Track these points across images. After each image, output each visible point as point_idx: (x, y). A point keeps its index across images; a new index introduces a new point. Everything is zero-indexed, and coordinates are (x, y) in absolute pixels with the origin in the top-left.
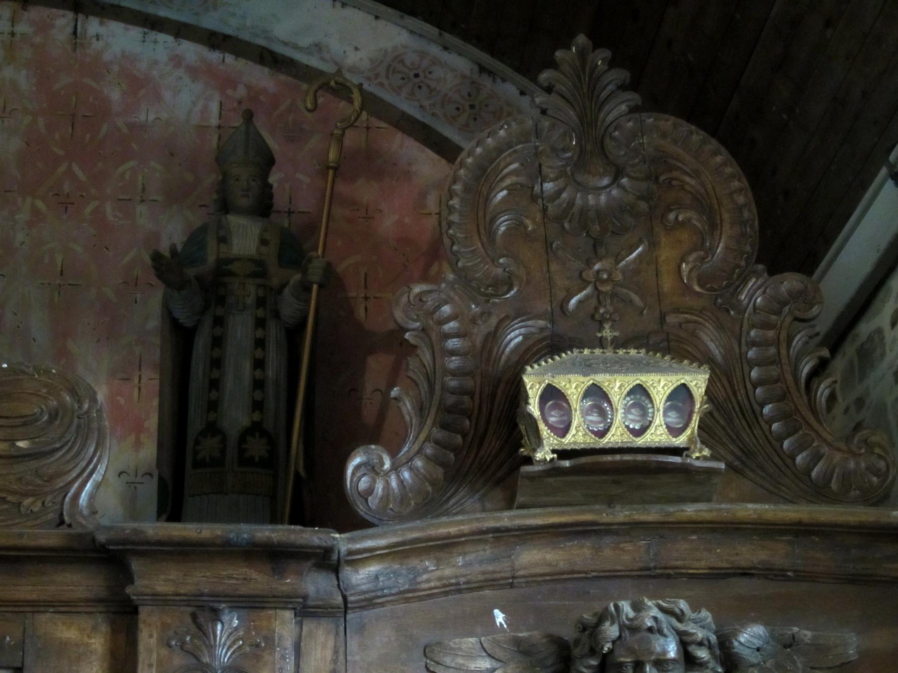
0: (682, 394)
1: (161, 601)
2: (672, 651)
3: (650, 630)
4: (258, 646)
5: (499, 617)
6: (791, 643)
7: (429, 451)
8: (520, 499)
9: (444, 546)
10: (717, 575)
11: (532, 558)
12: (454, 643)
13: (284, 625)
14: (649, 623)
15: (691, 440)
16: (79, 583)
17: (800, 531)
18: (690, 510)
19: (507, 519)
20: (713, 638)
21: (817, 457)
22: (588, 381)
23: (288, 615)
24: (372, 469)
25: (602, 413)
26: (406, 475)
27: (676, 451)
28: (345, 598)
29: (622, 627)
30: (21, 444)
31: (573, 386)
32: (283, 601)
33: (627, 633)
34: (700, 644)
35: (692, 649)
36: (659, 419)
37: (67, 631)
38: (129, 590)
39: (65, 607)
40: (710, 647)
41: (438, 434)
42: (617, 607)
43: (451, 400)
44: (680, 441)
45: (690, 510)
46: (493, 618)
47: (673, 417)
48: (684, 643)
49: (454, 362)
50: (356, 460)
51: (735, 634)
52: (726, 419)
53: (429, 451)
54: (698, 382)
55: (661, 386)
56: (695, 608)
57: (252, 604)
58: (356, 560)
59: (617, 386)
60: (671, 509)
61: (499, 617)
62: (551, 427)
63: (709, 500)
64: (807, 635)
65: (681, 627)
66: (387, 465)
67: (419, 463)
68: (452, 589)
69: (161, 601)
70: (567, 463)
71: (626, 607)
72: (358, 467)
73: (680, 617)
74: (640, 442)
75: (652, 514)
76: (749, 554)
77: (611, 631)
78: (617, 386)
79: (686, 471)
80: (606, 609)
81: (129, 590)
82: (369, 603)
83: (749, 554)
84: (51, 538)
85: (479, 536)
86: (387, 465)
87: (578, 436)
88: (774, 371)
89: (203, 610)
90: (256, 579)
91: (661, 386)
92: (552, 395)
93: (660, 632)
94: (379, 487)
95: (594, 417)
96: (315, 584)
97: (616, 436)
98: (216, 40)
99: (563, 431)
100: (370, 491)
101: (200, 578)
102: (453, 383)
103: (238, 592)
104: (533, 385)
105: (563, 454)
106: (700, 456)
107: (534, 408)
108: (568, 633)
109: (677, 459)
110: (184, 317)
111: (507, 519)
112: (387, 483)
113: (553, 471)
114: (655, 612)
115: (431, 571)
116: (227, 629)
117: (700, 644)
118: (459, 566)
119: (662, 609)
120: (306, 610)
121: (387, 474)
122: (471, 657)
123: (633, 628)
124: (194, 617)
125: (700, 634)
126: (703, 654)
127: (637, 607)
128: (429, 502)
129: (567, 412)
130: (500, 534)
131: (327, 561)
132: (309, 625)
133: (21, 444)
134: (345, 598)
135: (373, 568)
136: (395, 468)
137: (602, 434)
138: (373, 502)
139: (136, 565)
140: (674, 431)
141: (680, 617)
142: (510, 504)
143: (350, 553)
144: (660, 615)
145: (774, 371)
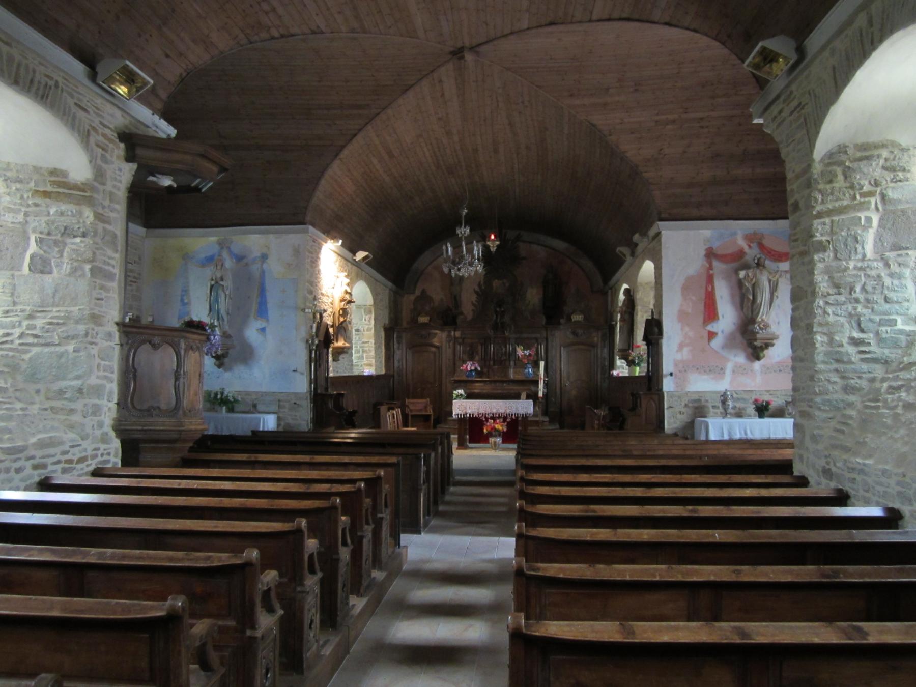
98: (546, 246)
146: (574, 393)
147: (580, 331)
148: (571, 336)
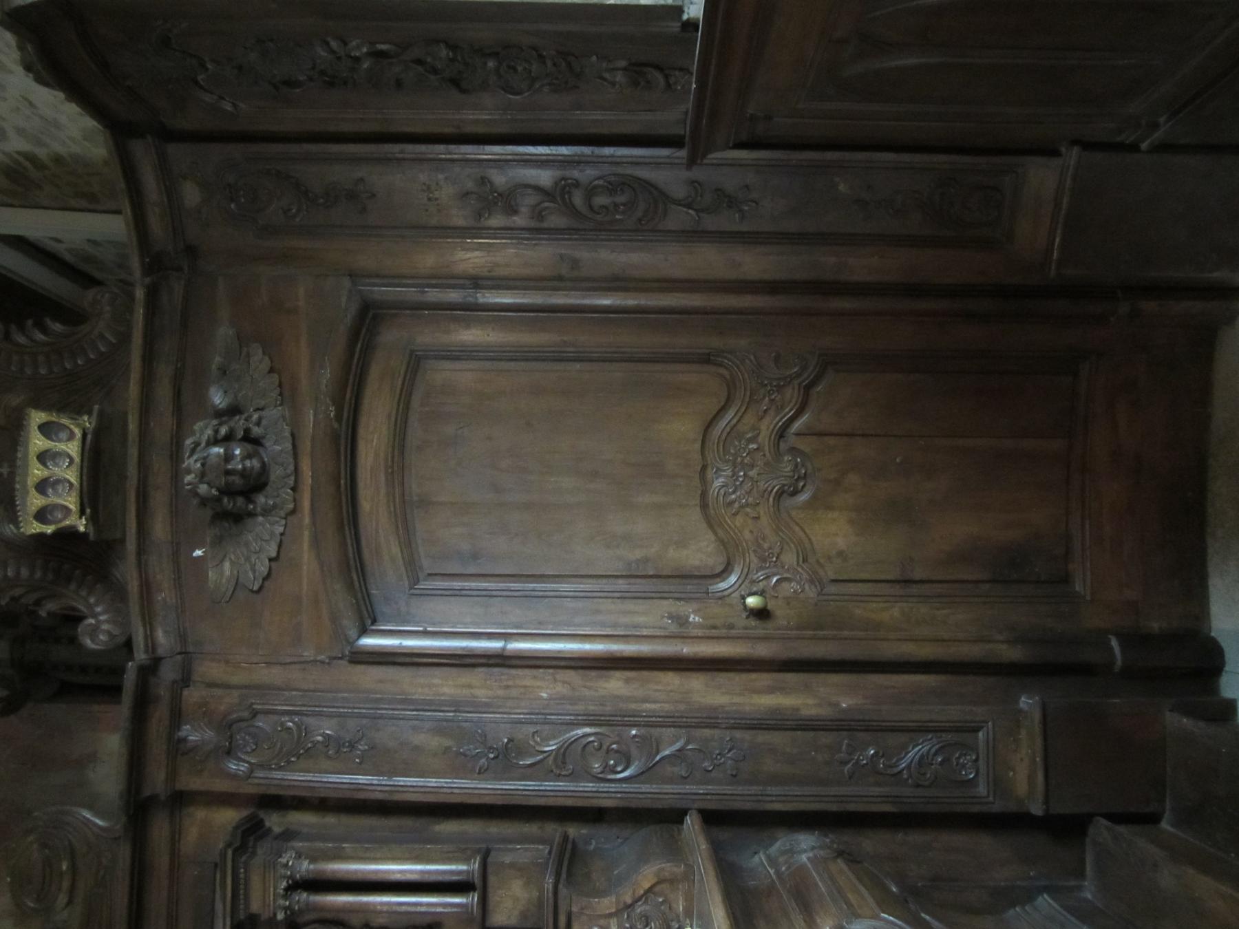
0: (45, 429)
1: (172, 775)
2: (218, 450)
3: (203, 465)
4: (204, 713)
5: (198, 553)
6: (223, 371)
7: (84, 593)
8: (118, 535)
9: (147, 588)
10: (178, 409)
11: (160, 528)
12: (211, 585)
13: (192, 695)
14: (199, 465)
15: (78, 425)
16: (159, 829)
17: (149, 358)
18: (132, 427)
19: (131, 545)
20: (215, 422)
21: (102, 336)
22: (33, 492)
23: (186, 692)
24: (94, 632)
25: (58, 482)
26: (99, 609)
27: (84, 436)
28: (180, 653)
29: (201, 482)
30: (64, 868)
31: (36, 501)
32: (176, 699)
33: (206, 479)
34: (216, 431)
35: (219, 437)
36: (62, 447)
37: (192, 834)
38: (163, 798)
39: (175, 839)
40: (220, 424)
41: (73, 586)
42: (189, 484)
43: (50, 576)
44: (78, 432)
45: (132, 427)
46: (199, 557)
47: (63, 435)
48: (216, 442)
49: (25, 572)
50: (88, 643)
51: (214, 406)
52: (65, 396)
53: (84, 593)
54: (38, 417)
55: (38, 442)
56: (193, 433)
57: (177, 717)
58: (151, 645)
59: (37, 472)
60: (130, 438)
61: (198, 553)
62: (65, 518)
63: (126, 414)
64: (218, 359)
65: (203, 445)
66: (92, 621)
67: (92, 600)
68: (178, 583)
69: (172, 775)
70: (88, 511)
71: (189, 478)
72: (93, 641)
73: (197, 444)
74: (77, 460)
75: (133, 452)
76: (164, 391)
77: (203, 489)
78: (37, 472)
79: (99, 432)
80: (190, 491)
81: (163, 798)
82: (183, 637)
83: (164, 391)
84: (124, 853)
85: (141, 565)
86: (92, 621)
87: (72, 502)
88: (41, 358)
89: (177, 748)
90: (159, 716)
91: (38, 442)
92: (41, 516)
93: (205, 458)
94: (105, 627)
95: (60, 488)
96: (168, 673)
97: (72, 476)
99: (67, 510)
100: (109, 632)
101: (157, 748)
102: (38, 574)
103: (493, 274)
104: (36, 528)
105: (82, 512)
106: (88, 422)
107: (50, 530)
108: (208, 513)
109: (89, 437)
111: (131, 545)
112: (104, 621)
113: (94, 520)
114: (192, 460)
115: (165, 595)
116: (192, 734)
117: (216, 431)
118: (162, 574)
119: (190, 457)
120: (186, 680)
121: (99, 622)
122: (222, 574)
123: (202, 476)
124: (184, 754)
125: (209, 432)
126: (223, 431)
127: (189, 472)
128: (118, 594)
129: (56, 507)
130: (141, 551)
131: (150, 670)
132: (195, 677)
133: (64, 868)
134: (180, 653)
135: (160, 635)
136: (95, 616)
137: (71, 485)
138: (116, 631)
139: (147, 792)
140: (71, 436)
141: (197, 444)
142: (123, 541)
143: (146, 652)
144: (195, 457)
145: (41, 358)
146: (834, 533)
147: (206, 454)
148: (263, 536)
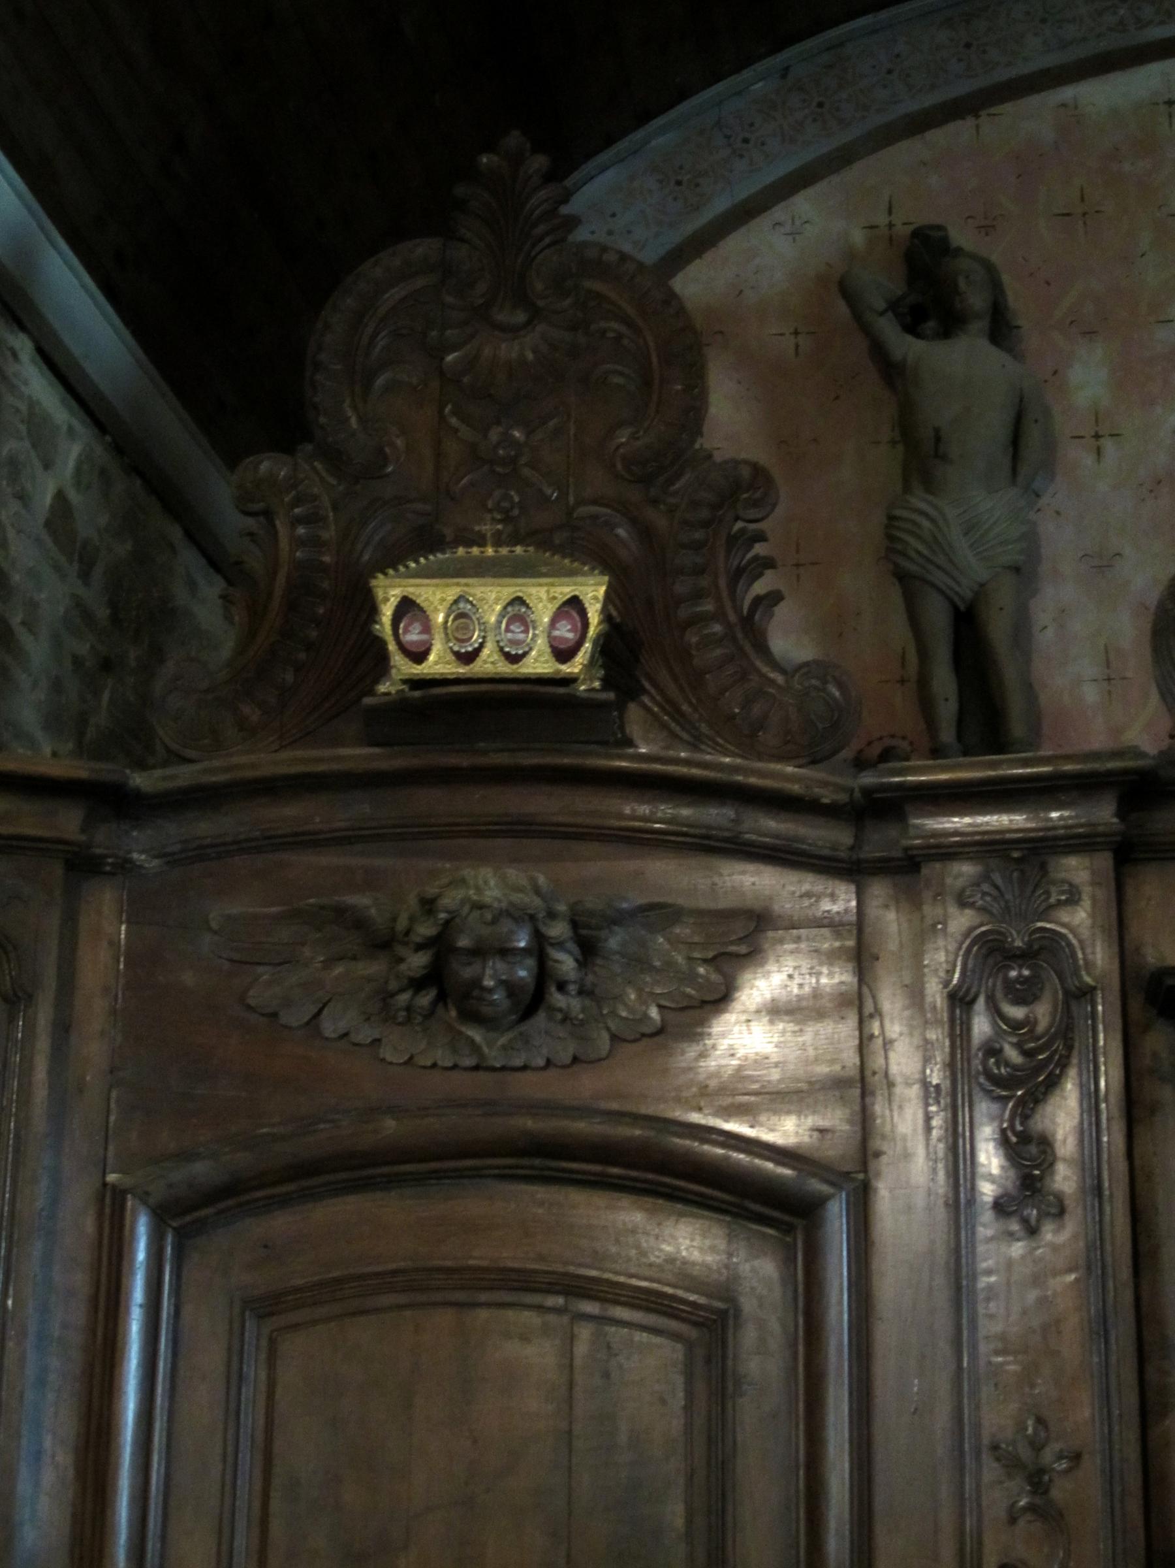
110: (907, 981)
